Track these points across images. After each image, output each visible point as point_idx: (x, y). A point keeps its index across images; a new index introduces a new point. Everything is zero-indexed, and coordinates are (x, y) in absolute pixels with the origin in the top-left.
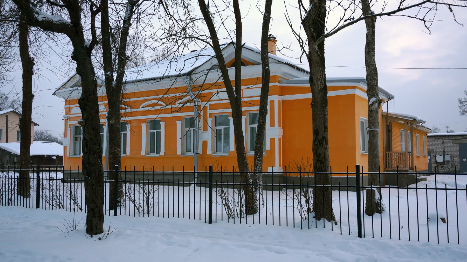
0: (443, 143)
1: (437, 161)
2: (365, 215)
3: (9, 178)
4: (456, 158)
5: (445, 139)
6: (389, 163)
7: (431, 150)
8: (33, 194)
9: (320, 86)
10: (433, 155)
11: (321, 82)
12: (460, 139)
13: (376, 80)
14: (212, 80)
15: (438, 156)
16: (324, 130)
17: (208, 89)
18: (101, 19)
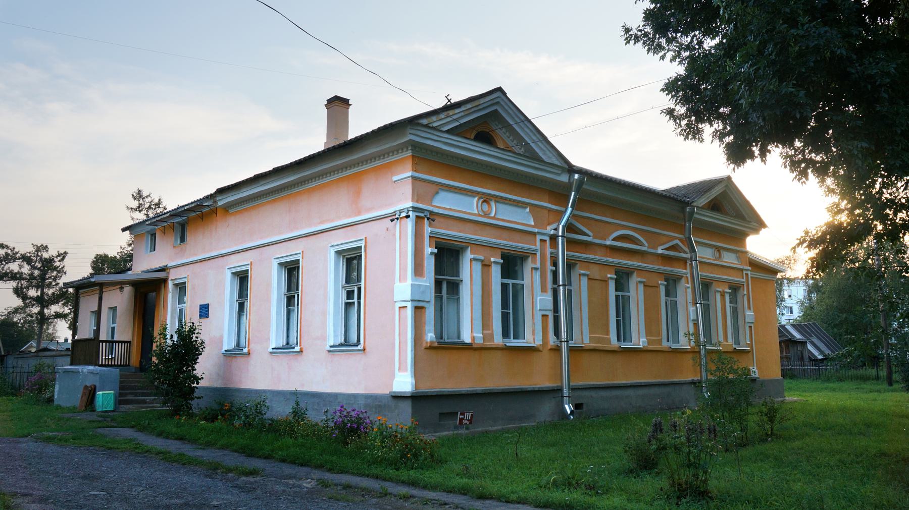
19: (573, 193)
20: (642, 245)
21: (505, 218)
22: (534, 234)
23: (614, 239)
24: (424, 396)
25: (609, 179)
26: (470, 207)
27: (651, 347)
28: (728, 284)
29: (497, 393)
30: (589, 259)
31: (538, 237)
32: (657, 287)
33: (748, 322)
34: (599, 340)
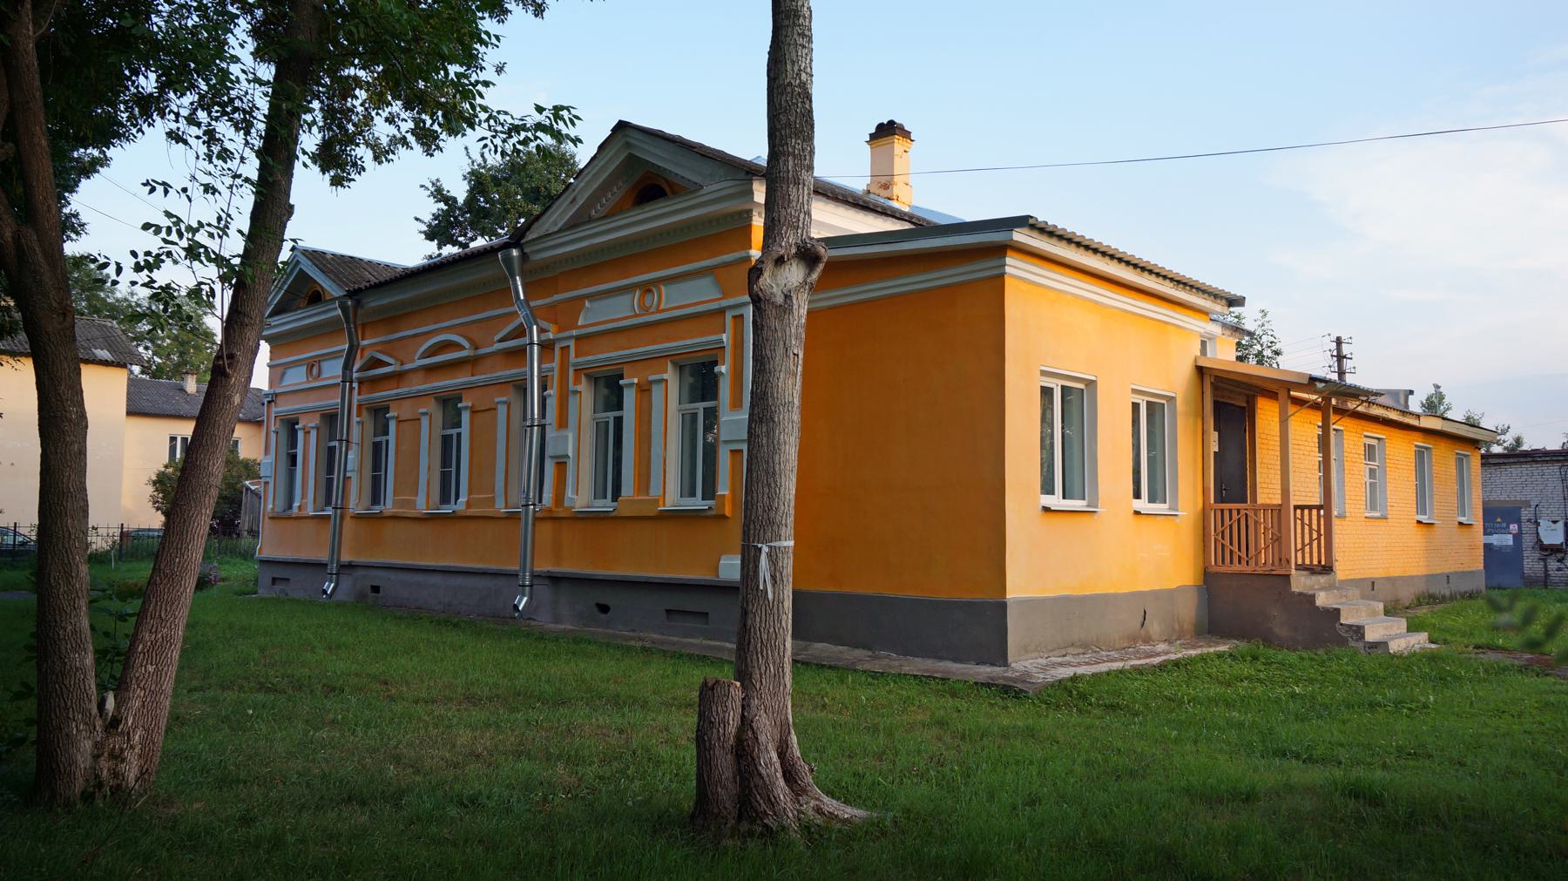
1: (1542, 539)
2: (284, 384)
6: (1231, 552)
7: (1521, 501)
8: (295, 260)
10: (1529, 520)
13: (795, 157)
15: (1544, 524)
17: (386, 276)
18: (846, 589)
19: (518, 278)
20: (459, 347)
21: (613, 318)
22: (721, 312)
23: (423, 356)
24: (729, 587)
25: (482, 250)
26: (618, 310)
27: (473, 511)
28: (432, 397)
29: (725, 587)
30: (397, 395)
31: (729, 316)
32: (495, 409)
33: (726, 442)
34: (404, 504)
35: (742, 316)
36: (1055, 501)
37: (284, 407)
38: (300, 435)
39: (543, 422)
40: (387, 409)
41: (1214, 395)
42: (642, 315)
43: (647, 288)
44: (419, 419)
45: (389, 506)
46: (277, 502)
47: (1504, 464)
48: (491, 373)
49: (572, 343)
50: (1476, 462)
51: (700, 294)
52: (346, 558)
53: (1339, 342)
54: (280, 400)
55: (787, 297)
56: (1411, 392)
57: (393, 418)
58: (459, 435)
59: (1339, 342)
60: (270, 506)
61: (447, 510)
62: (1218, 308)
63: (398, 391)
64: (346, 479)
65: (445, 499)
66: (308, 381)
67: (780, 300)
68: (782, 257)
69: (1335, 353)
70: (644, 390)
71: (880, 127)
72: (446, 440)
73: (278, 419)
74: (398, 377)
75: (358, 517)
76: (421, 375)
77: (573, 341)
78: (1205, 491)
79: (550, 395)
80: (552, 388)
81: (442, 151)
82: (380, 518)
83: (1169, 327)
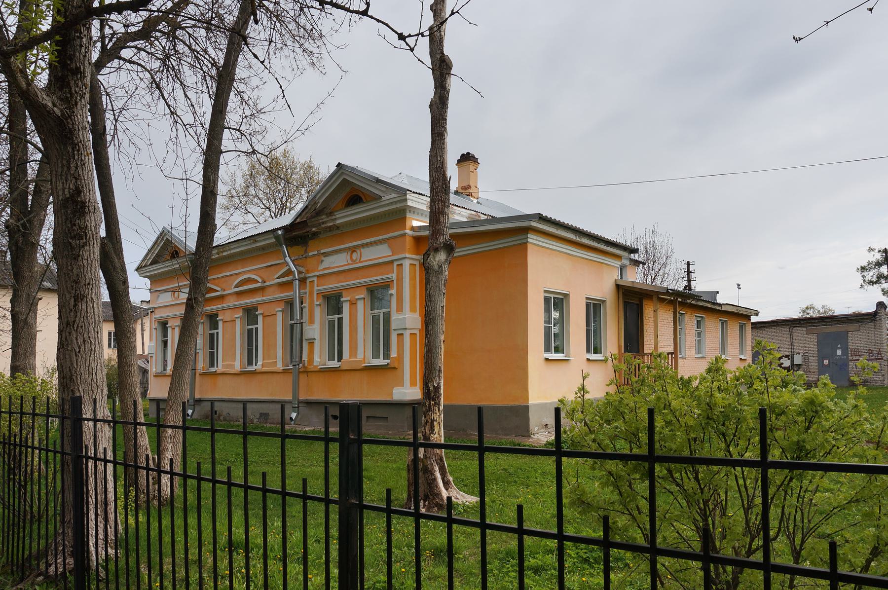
0: (791, 334)
3: (246, 487)
4: (812, 359)
5: (794, 327)
9: (60, 193)
11: (63, 183)
12: (819, 326)
13: (442, 202)
14: (420, 214)
16: (72, 307)
20: (256, 281)
22: (392, 262)
27: (265, 369)
30: (222, 307)
31: (395, 264)
34: (228, 366)
35: (401, 265)
36: (553, 356)
37: (161, 314)
38: (170, 330)
39: (302, 321)
40: (217, 315)
41: (624, 298)
42: (352, 264)
43: (353, 250)
44: (235, 321)
45: (220, 368)
46: (157, 367)
47: (764, 327)
48: (273, 295)
49: (315, 279)
50: (749, 328)
51: (379, 253)
52: (197, 396)
53: (688, 264)
54: (157, 311)
55: (440, 267)
56: (718, 292)
57: (220, 320)
58: (257, 329)
59: (688, 264)
60: (154, 370)
61: (250, 368)
62: (624, 254)
63: (223, 305)
64: (196, 353)
65: (250, 363)
66: (173, 301)
67: (436, 268)
68: (438, 248)
69: (686, 270)
70: (353, 303)
71: (463, 155)
72: (250, 332)
73: (156, 322)
74: (222, 297)
75: (203, 374)
76: (234, 297)
77: (316, 278)
78: (619, 347)
79: (305, 307)
80: (306, 303)
81: (607, 385)
82: (215, 374)
83: (603, 265)
